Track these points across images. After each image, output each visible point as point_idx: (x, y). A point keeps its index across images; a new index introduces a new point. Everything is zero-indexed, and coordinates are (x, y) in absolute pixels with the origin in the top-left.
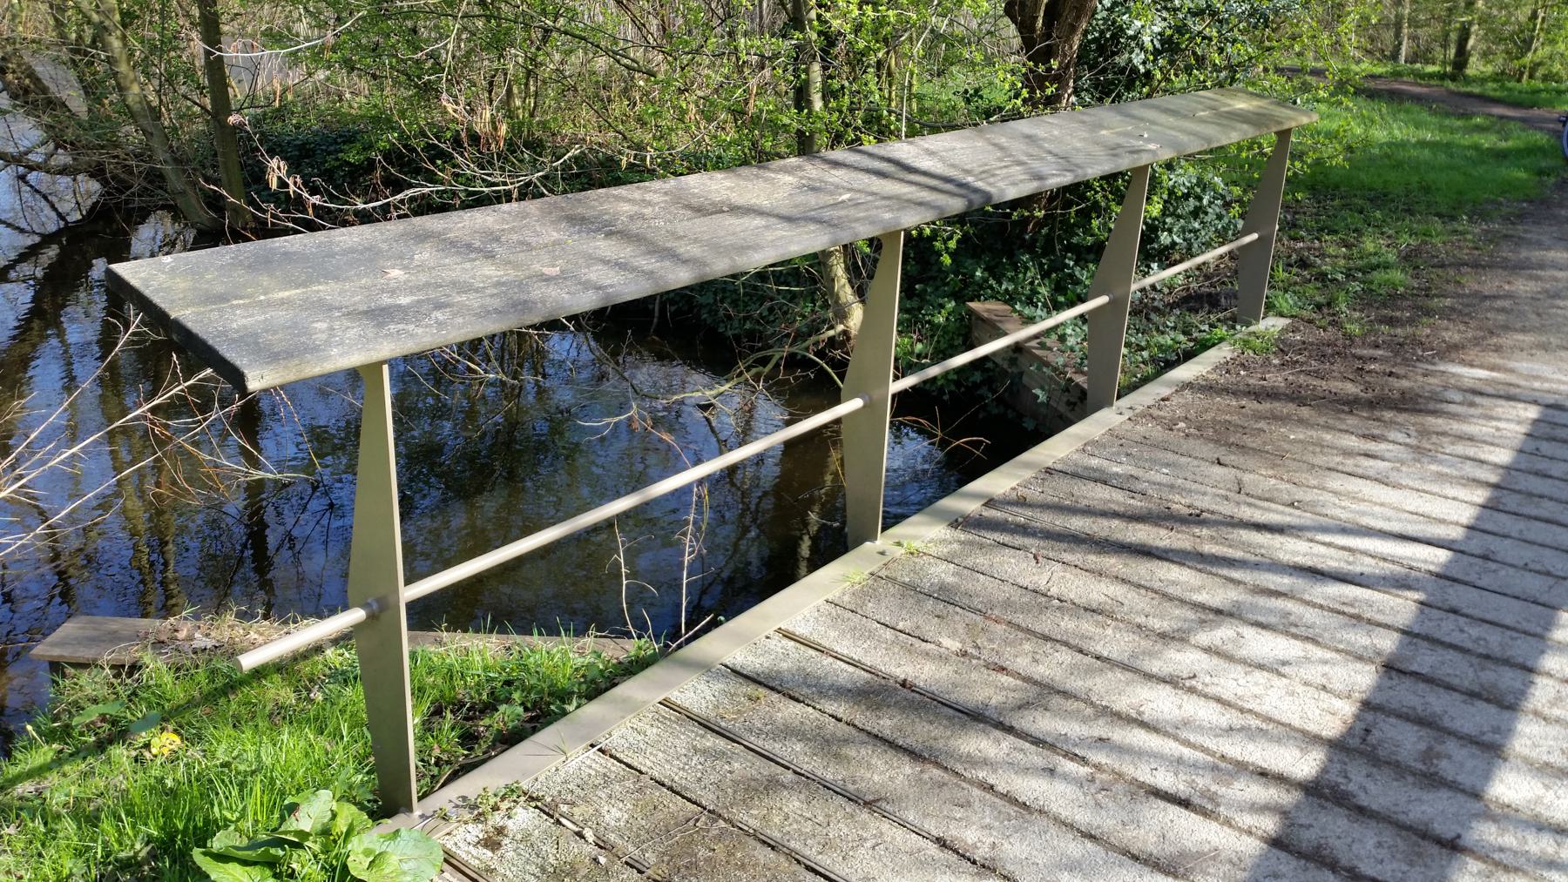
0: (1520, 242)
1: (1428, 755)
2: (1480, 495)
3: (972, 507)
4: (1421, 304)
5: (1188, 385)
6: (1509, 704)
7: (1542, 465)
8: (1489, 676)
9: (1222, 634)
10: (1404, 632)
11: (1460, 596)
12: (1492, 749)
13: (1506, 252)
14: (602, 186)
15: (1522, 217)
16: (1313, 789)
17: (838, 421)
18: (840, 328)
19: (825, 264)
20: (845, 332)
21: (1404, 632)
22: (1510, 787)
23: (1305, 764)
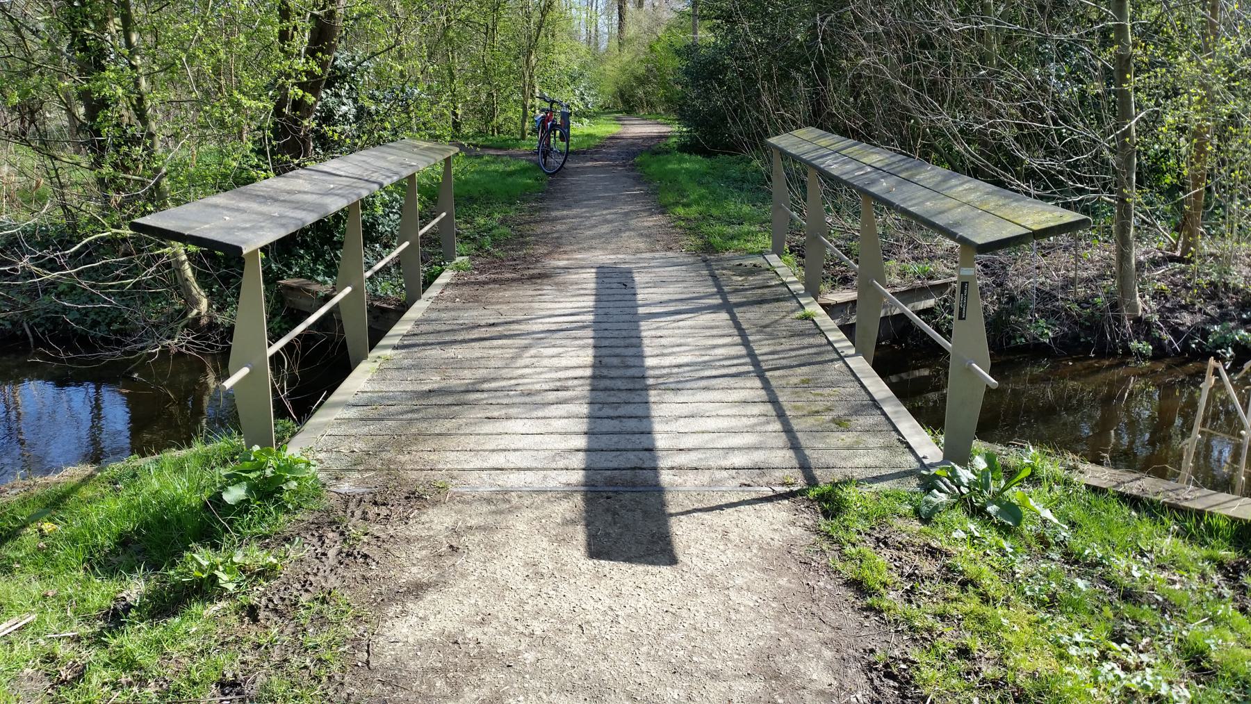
0: (549, 210)
1: (622, 362)
2: (593, 298)
3: (396, 341)
4: (520, 240)
5: (447, 285)
6: (640, 346)
7: (608, 383)
8: (628, 341)
9: (533, 352)
10: (586, 451)
11: (604, 326)
12: (641, 356)
13: (544, 214)
14: (845, 132)
15: (542, 199)
16: (593, 377)
17: (337, 304)
18: (195, 311)
19: (179, 270)
20: (198, 314)
21: (586, 451)
22: (649, 362)
23: (588, 372)
